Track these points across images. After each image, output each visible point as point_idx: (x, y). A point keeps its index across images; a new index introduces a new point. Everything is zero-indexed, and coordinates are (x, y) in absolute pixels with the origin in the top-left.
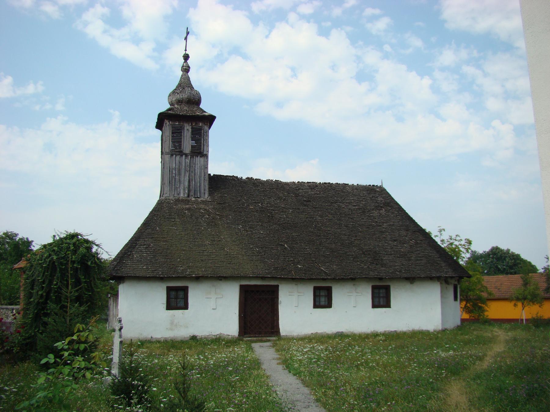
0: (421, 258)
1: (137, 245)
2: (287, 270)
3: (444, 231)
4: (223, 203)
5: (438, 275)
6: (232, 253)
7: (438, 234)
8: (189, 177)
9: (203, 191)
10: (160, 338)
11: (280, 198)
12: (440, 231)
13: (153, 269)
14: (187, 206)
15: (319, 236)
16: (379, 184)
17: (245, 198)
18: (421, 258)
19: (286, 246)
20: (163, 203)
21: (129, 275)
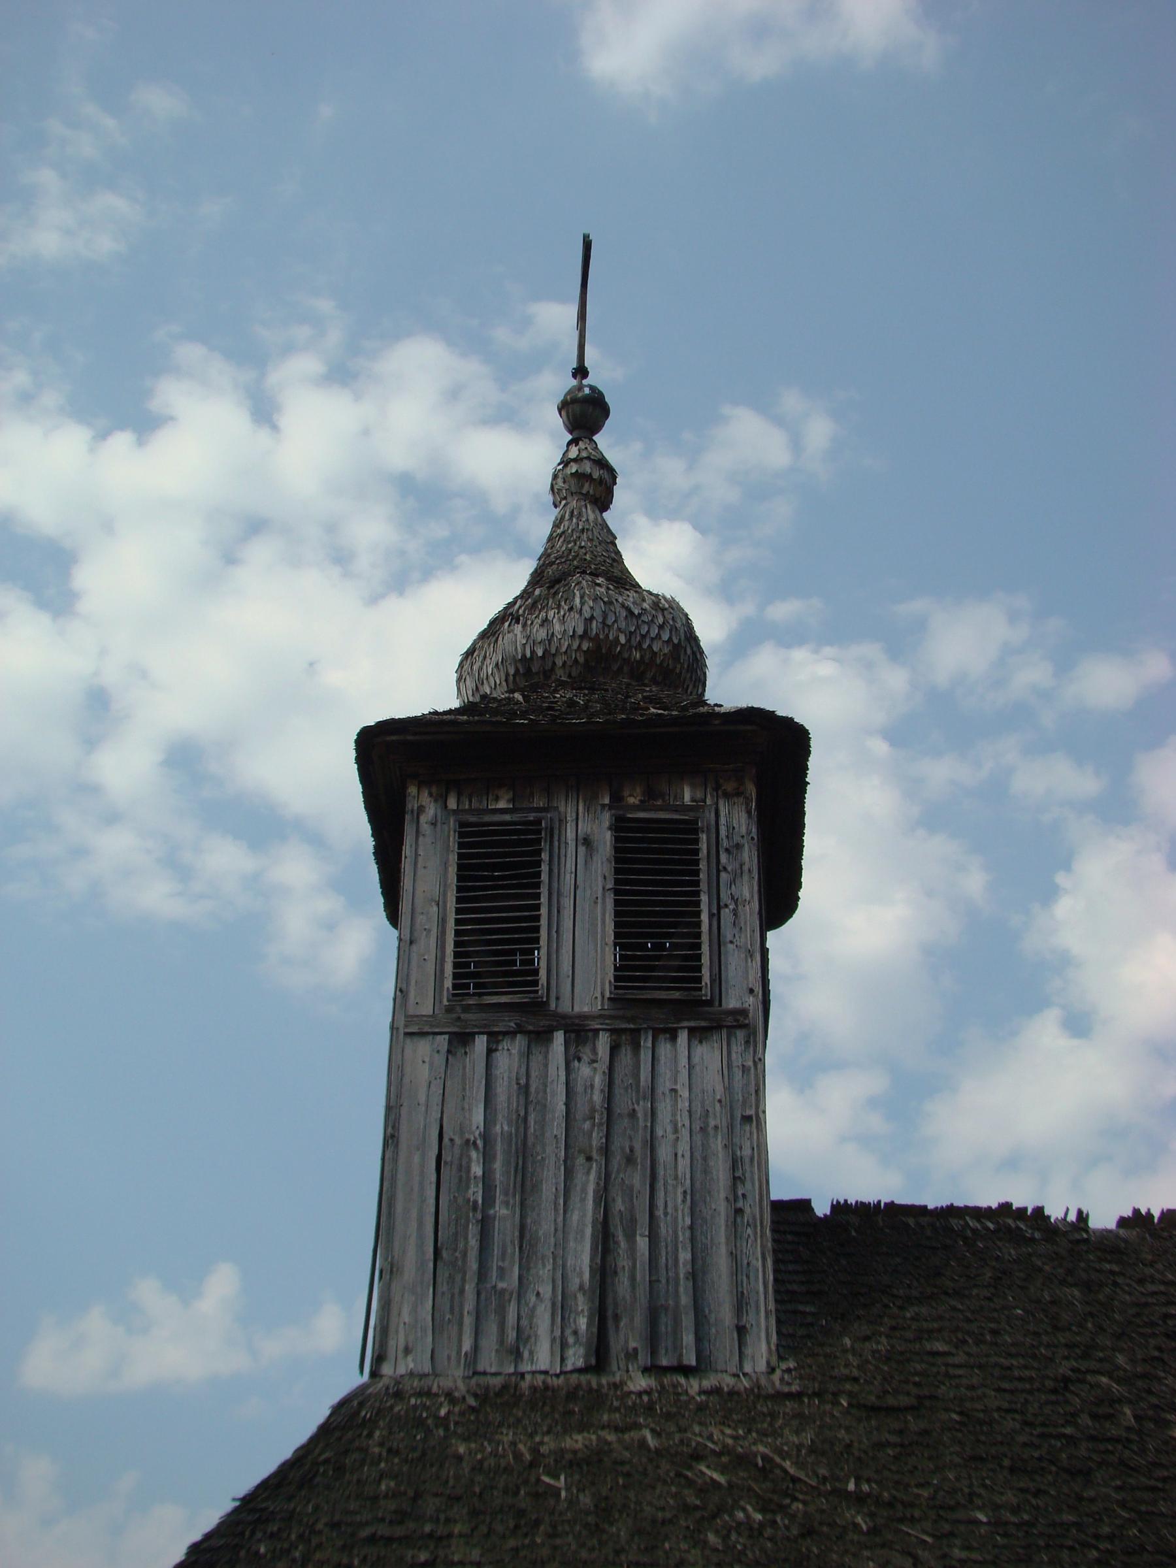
4: (904, 1401)
9: (724, 1313)
14: (577, 1441)
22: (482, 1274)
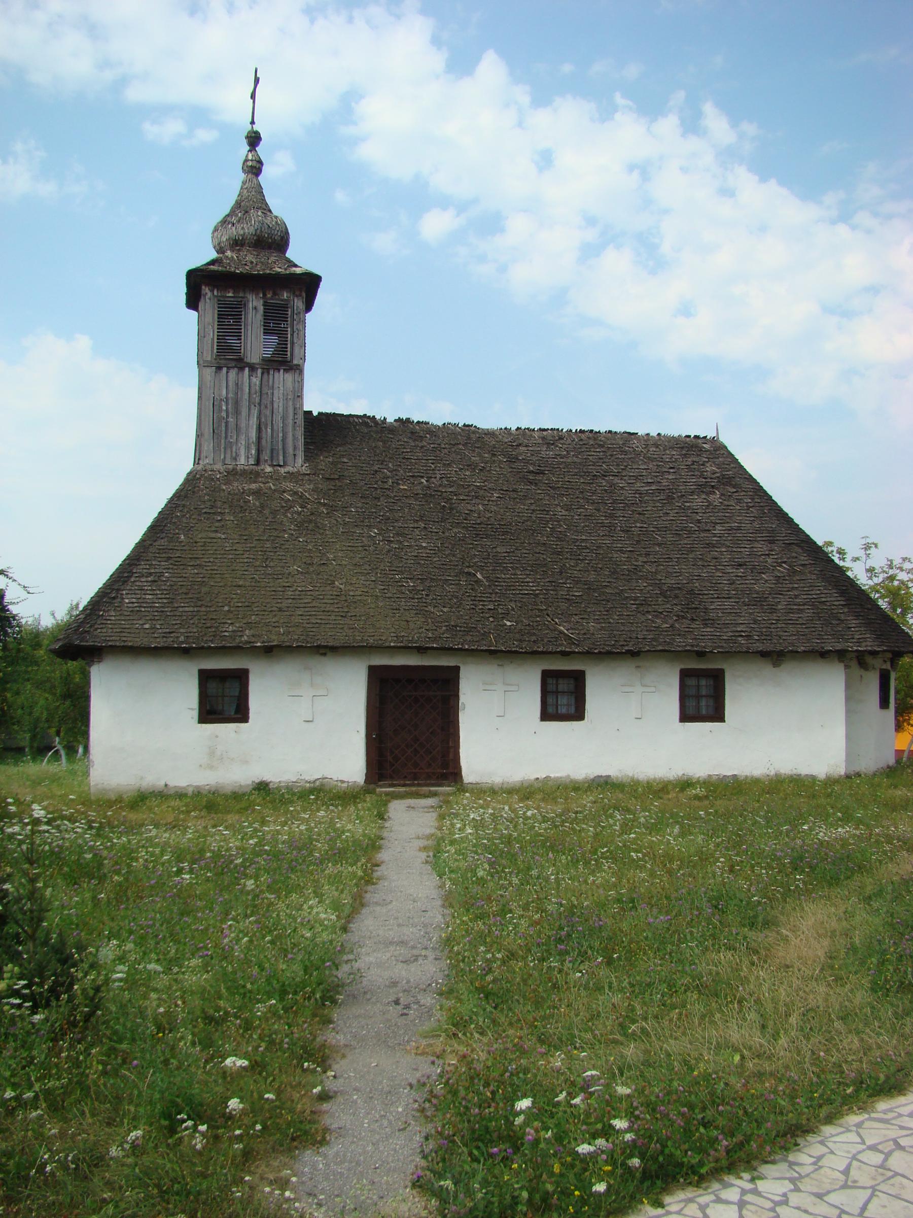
0: (801, 607)
1: (131, 577)
2: (479, 632)
3: (876, 546)
4: (337, 477)
5: (839, 647)
6: (351, 593)
7: (861, 554)
8: (259, 418)
9: (290, 450)
10: (184, 788)
11: (472, 466)
12: (867, 547)
13: (165, 630)
14: (254, 486)
15: (559, 553)
16: (711, 434)
17: (390, 465)
18: (801, 607)
19: (479, 576)
20: (198, 479)
21: (110, 643)
22: (226, 437)
